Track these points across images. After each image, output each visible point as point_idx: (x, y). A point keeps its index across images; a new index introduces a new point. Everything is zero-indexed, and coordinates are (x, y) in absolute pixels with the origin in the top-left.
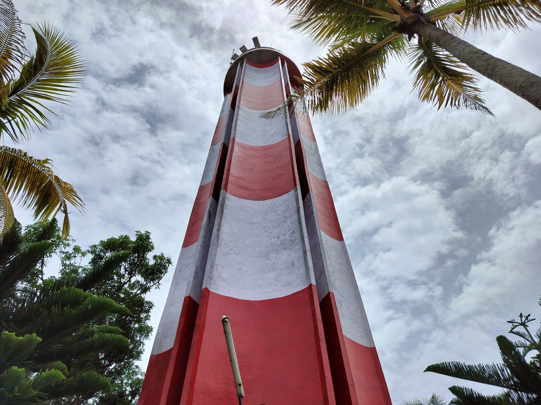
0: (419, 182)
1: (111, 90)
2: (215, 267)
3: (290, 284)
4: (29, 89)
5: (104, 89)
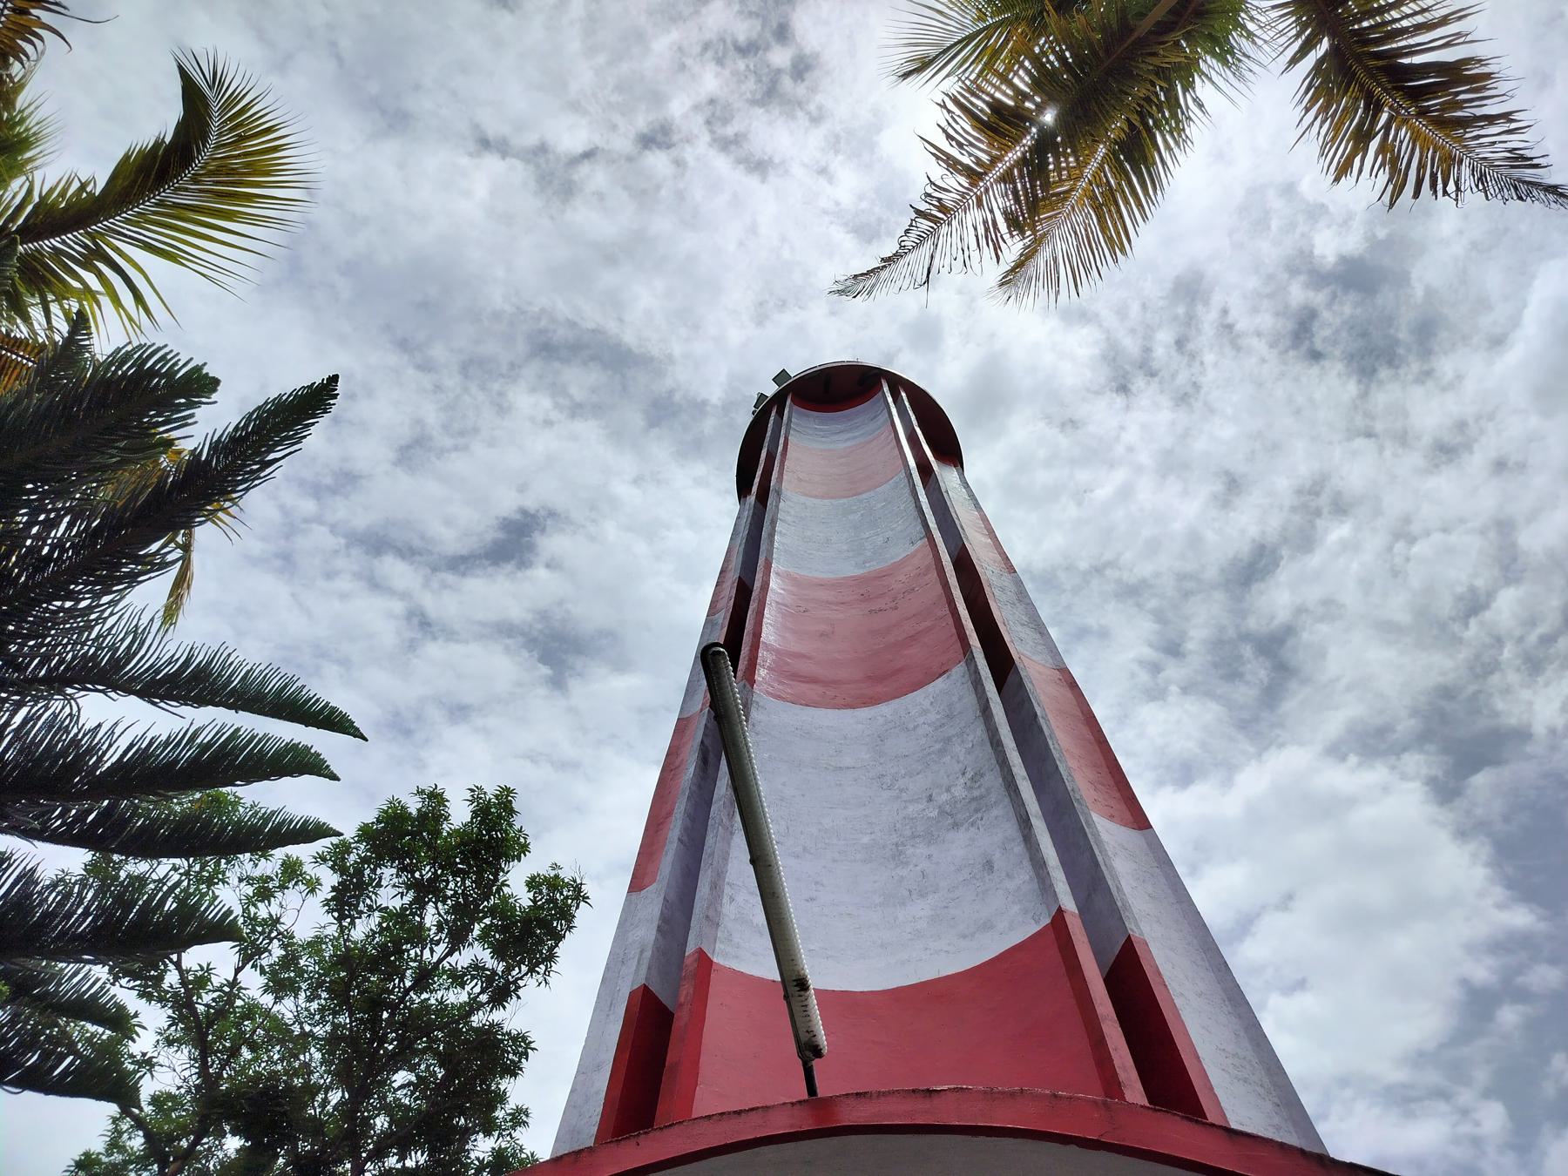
0: (1353, 759)
1: (444, 586)
2: (727, 890)
3: (987, 926)
4: (127, 221)
5: (426, 585)
